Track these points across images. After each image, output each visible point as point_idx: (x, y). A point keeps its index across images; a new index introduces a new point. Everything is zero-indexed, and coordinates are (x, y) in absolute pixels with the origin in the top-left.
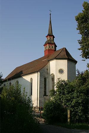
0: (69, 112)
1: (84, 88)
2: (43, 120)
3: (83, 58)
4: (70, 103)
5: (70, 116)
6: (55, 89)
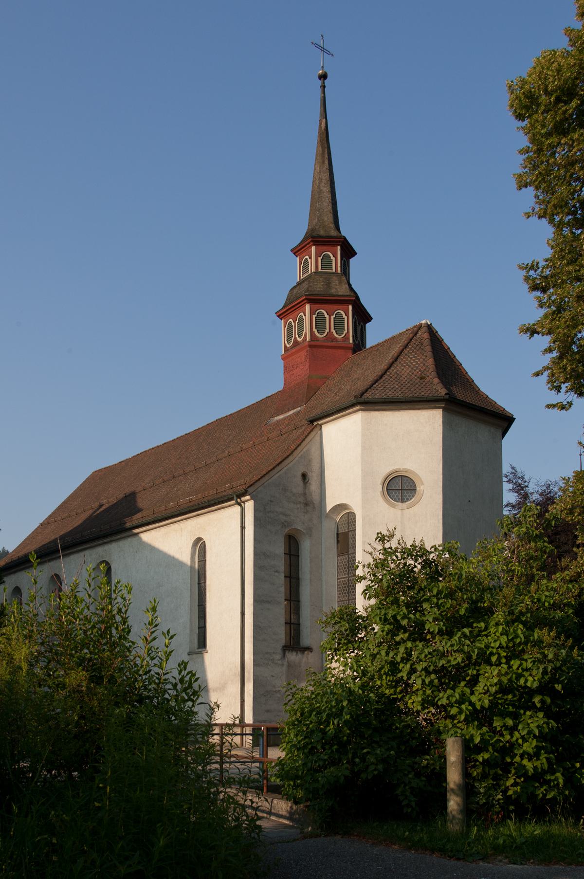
0: (453, 753)
1: (555, 590)
2: (282, 806)
3: (558, 389)
4: (463, 694)
5: (466, 774)
6: (362, 604)
